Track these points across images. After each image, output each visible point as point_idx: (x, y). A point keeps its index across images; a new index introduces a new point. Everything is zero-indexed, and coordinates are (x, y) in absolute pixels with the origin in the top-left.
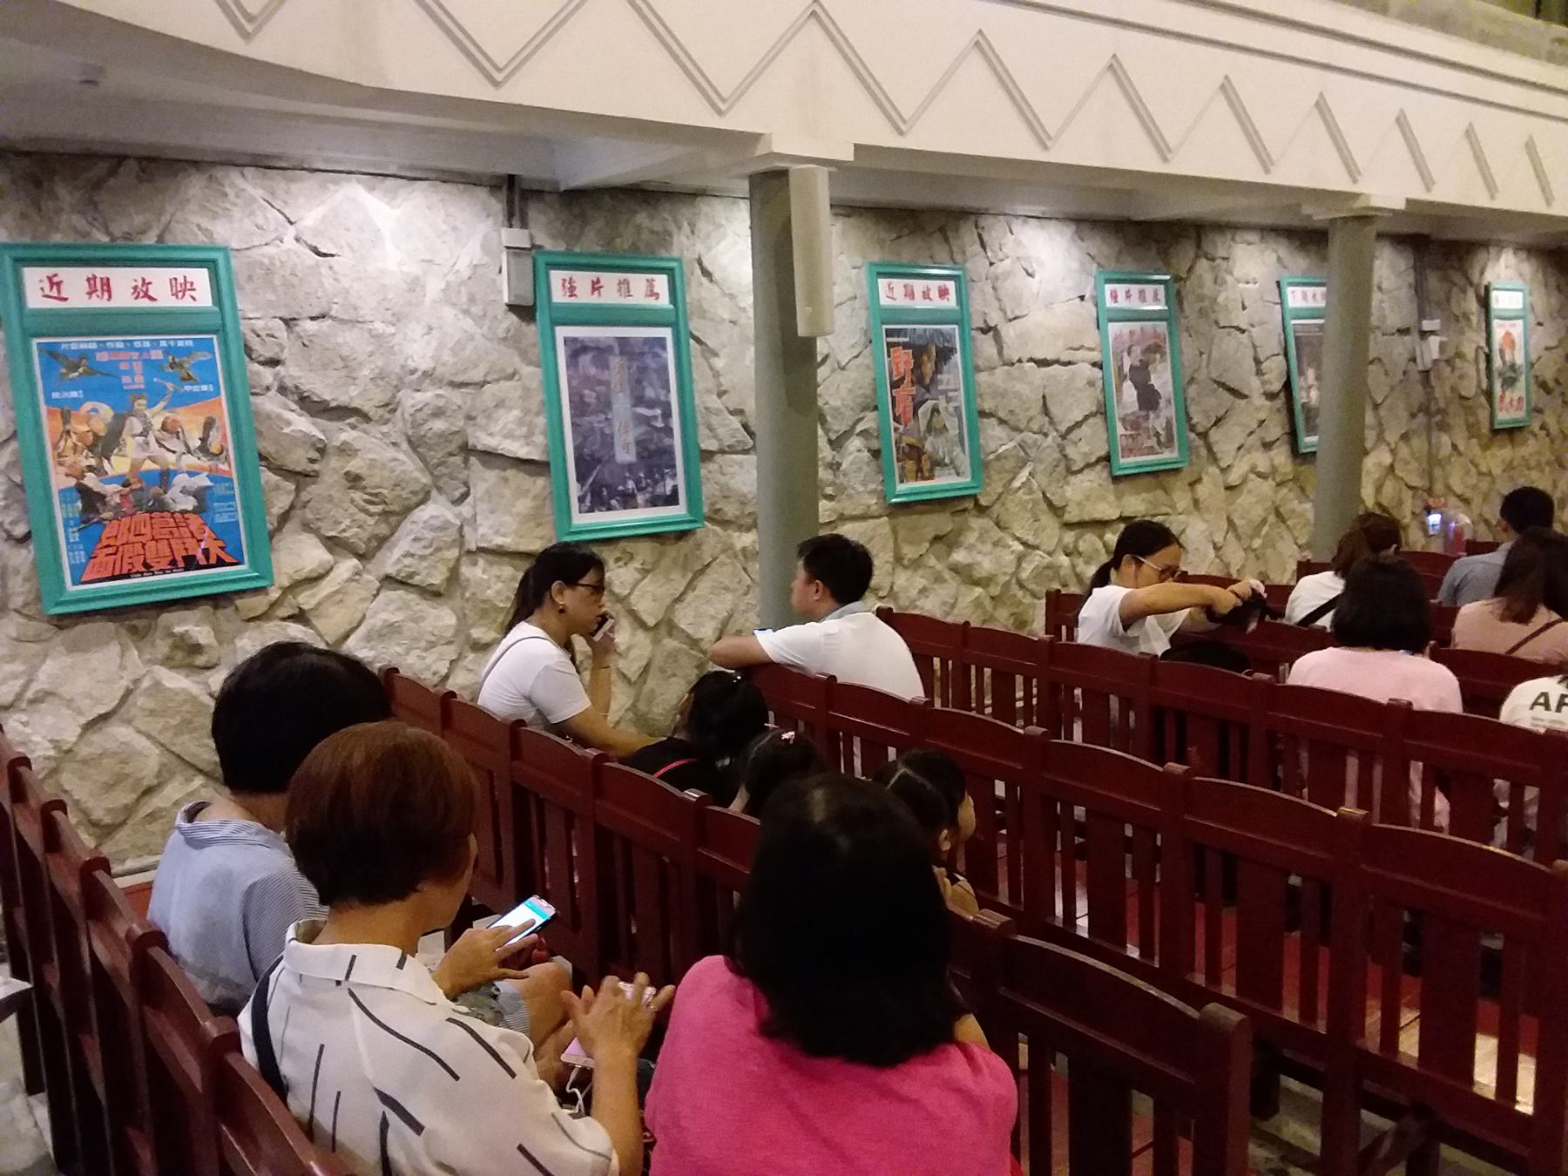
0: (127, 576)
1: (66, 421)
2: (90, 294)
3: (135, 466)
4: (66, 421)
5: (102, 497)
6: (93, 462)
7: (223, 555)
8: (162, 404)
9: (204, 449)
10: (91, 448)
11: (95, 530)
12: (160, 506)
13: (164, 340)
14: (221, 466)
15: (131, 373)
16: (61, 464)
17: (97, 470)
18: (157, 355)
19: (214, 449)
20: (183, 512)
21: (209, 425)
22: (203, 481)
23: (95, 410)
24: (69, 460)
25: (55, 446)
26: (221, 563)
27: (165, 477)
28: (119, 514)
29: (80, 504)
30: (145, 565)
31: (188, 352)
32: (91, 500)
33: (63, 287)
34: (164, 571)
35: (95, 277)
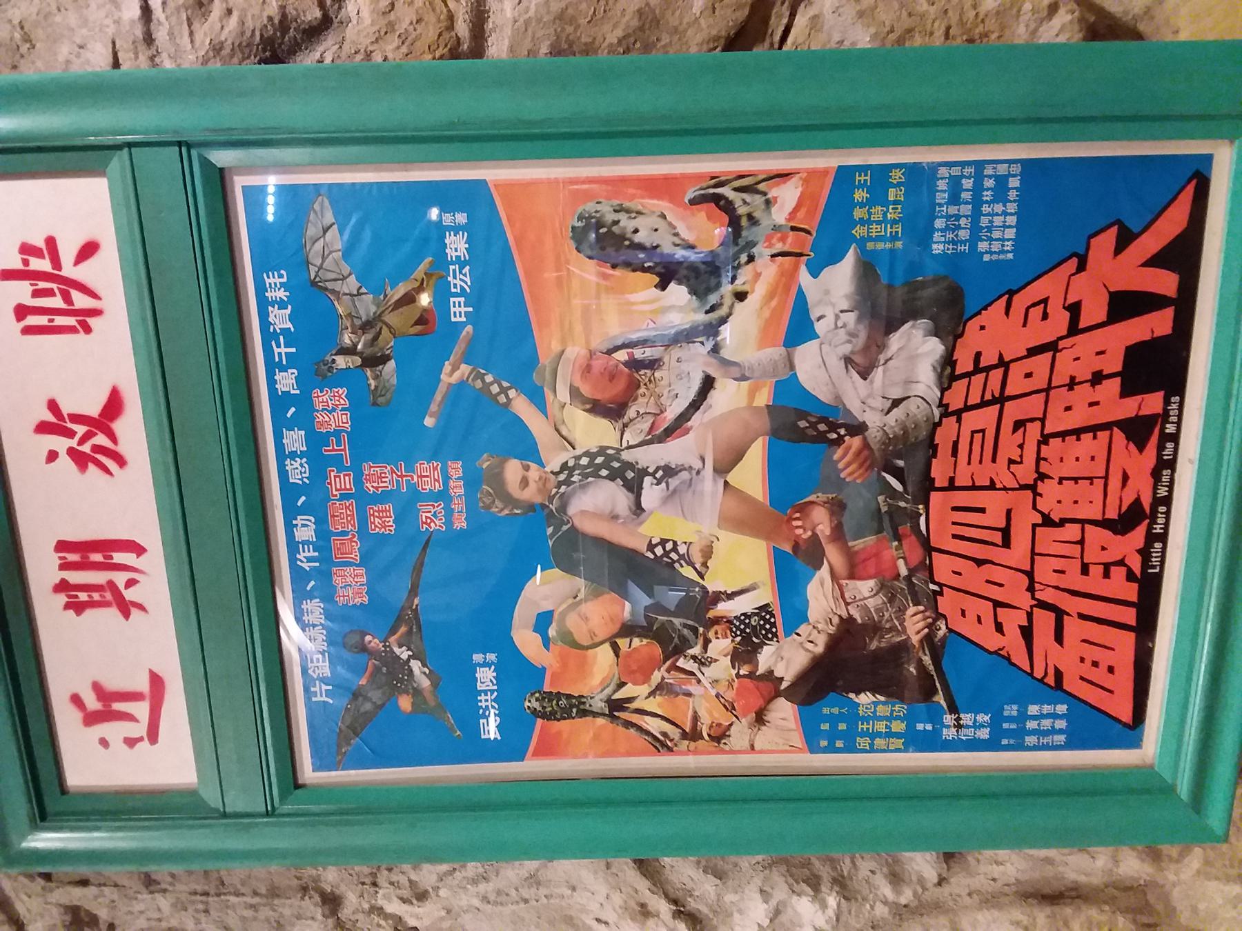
0: (1149, 588)
1: (577, 707)
2: (125, 608)
3: (745, 519)
4: (577, 707)
5: (847, 634)
6: (721, 646)
7: (1150, 243)
8: (522, 407)
9: (702, 277)
10: (673, 647)
11: (962, 670)
12: (910, 461)
13: (274, 380)
14: (779, 215)
15: (407, 504)
16: (719, 736)
17: (752, 634)
18: (333, 409)
19: (704, 233)
20: (948, 372)
21: (609, 244)
22: (834, 289)
23: (543, 622)
24: (710, 715)
25: (661, 745)
26: (1183, 255)
27: (801, 427)
28: (920, 588)
29: (865, 699)
30: (1122, 524)
31: (312, 292)
32: (849, 664)
33: (114, 683)
34: (1165, 465)
35: (62, 587)
